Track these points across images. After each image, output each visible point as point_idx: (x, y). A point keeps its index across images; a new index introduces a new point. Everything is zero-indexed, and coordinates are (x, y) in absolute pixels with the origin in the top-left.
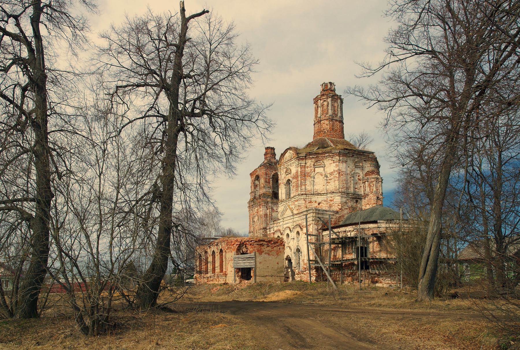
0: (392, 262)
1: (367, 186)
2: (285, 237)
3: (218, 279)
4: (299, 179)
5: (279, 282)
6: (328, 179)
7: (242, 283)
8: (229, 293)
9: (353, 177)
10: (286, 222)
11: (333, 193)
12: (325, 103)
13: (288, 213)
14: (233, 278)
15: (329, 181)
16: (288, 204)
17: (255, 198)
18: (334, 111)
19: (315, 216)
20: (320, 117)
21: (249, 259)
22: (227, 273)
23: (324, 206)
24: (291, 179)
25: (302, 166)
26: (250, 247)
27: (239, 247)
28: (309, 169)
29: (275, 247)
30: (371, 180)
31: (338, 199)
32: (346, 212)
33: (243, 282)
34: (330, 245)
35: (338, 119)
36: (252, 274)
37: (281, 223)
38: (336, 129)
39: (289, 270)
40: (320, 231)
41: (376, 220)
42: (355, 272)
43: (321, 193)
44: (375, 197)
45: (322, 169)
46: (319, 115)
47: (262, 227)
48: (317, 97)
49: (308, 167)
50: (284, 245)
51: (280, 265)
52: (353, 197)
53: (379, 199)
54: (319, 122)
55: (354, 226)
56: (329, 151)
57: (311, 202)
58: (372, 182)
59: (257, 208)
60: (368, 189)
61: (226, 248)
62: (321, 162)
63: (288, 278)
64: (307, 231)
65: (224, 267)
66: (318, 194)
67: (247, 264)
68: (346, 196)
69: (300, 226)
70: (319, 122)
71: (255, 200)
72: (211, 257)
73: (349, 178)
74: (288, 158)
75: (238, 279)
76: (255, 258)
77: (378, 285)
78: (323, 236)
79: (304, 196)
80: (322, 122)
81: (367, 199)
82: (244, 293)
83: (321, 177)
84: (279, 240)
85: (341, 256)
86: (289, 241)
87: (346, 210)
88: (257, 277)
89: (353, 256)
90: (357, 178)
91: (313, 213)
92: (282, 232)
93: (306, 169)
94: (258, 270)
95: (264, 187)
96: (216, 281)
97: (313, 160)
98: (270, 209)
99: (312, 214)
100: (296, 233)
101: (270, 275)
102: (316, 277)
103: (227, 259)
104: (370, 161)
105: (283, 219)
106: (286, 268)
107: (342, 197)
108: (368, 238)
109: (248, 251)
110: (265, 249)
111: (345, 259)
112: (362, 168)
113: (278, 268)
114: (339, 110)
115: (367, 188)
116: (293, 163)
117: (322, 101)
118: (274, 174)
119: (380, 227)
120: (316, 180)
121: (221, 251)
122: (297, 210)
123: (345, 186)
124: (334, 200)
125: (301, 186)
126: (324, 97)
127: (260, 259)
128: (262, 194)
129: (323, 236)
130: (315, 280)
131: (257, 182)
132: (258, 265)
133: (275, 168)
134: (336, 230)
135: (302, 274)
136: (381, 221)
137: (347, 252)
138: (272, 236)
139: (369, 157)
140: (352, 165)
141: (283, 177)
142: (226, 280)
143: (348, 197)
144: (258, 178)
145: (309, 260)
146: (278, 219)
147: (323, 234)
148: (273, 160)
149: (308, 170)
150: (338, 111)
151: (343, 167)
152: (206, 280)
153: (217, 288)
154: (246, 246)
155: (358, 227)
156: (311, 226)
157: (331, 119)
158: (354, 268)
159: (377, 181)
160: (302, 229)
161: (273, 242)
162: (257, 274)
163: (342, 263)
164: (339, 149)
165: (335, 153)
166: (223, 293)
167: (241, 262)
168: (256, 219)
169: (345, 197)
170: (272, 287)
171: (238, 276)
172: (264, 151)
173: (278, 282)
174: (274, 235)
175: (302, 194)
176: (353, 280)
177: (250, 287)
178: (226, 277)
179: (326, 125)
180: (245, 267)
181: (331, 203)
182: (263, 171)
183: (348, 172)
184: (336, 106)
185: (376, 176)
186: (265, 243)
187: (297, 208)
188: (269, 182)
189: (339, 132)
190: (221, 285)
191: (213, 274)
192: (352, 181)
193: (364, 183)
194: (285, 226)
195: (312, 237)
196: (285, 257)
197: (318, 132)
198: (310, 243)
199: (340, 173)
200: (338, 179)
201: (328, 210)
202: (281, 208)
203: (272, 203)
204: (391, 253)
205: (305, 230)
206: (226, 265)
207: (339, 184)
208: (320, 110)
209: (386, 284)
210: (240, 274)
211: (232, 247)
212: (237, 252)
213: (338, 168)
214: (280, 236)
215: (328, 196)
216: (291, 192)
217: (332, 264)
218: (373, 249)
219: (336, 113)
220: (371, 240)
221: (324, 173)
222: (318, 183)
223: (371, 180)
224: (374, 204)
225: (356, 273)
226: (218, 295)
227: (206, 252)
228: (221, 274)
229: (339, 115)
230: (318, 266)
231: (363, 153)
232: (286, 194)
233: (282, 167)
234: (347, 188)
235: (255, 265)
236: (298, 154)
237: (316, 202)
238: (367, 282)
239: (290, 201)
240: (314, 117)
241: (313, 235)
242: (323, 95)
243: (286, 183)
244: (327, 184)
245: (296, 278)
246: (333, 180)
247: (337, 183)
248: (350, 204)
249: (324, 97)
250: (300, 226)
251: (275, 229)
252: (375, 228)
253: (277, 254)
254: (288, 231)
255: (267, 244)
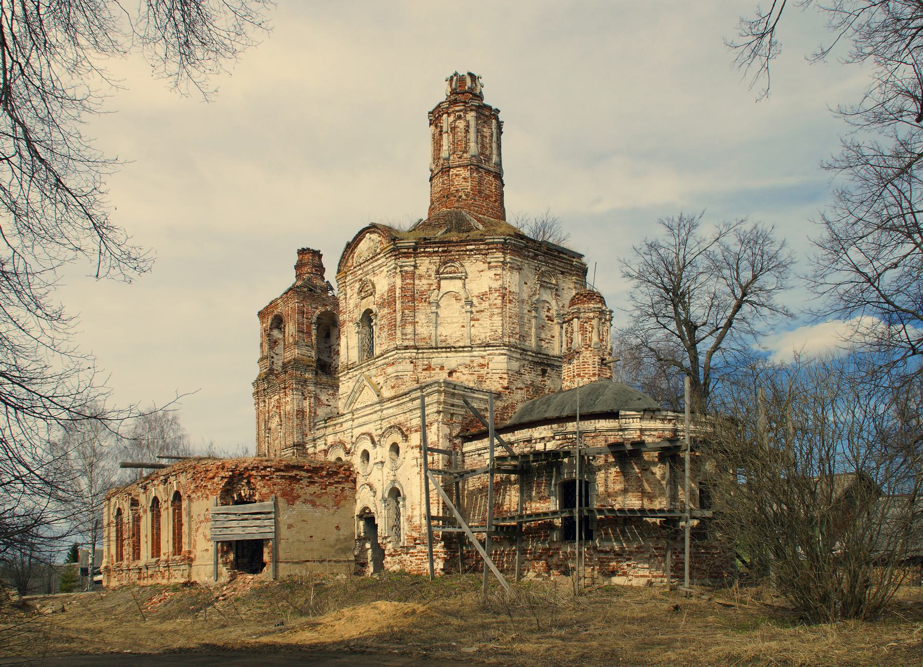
0: (654, 520)
1: (576, 329)
2: (356, 460)
3: (167, 573)
4: (398, 306)
5: (342, 577)
6: (474, 310)
7: (237, 583)
8: (198, 610)
9: (536, 309)
10: (362, 420)
11: (488, 345)
12: (461, 124)
13: (368, 396)
14: (211, 568)
15: (477, 316)
16: (367, 373)
17: (271, 371)
18: (483, 146)
19: (445, 402)
20: (448, 159)
21: (259, 516)
22: (192, 556)
23: (464, 378)
24: (374, 308)
25: (406, 272)
26: (261, 483)
27: (228, 483)
28: (424, 281)
29: (331, 484)
30: (587, 315)
31: (499, 363)
32: (519, 395)
33: (240, 578)
34: (492, 475)
35: (492, 169)
36: (266, 557)
37: (346, 425)
38: (487, 192)
39: (368, 545)
40: (457, 441)
41: (615, 408)
42: (556, 546)
43: (457, 345)
44: (597, 359)
45: (459, 283)
46: (444, 154)
47: (290, 442)
48: (439, 106)
49: (420, 277)
50: (354, 481)
51: (344, 532)
52: (536, 360)
53: (605, 365)
54: (445, 170)
55: (555, 426)
56: (479, 237)
57: (428, 368)
58: (590, 319)
59: (277, 397)
60: (578, 338)
61: (192, 487)
62: (457, 264)
63: (364, 565)
64: (424, 438)
65: (185, 539)
66: (450, 348)
67: (254, 530)
68: (518, 356)
69: (400, 429)
70: (445, 170)
71: (272, 377)
72: (149, 514)
73: (526, 311)
74: (366, 255)
75: (224, 571)
76: (276, 512)
77: (617, 580)
78: (463, 454)
79: (412, 353)
80: (453, 172)
81: (575, 361)
82: (243, 609)
83: (457, 306)
84: (341, 467)
85: (514, 506)
86: (369, 469)
87: (519, 391)
88: (281, 566)
89: (553, 505)
90: (544, 314)
91: (439, 392)
92: (348, 446)
93: (417, 282)
94: (282, 545)
95: (296, 343)
96: (163, 578)
97: (436, 259)
98: (312, 399)
99: (435, 397)
100: (388, 447)
101: (316, 558)
102: (445, 560)
103: (195, 517)
104: (573, 275)
105: (352, 412)
106: (360, 539)
107: (510, 358)
108: (594, 458)
109: (254, 495)
110: (306, 490)
111: (528, 512)
112: (557, 291)
113: (338, 540)
114: (494, 145)
115: (575, 334)
116: (380, 266)
117: (452, 118)
118: (322, 313)
119: (626, 429)
120: (443, 313)
121: (177, 496)
122: (393, 388)
123: (517, 330)
124: (491, 366)
125: (403, 326)
126: (457, 108)
127: (289, 517)
128: (289, 362)
129: (463, 454)
130: (443, 570)
131: (276, 333)
132: (284, 532)
133: (324, 300)
134: (506, 437)
135: (403, 555)
136: (628, 413)
137: (534, 493)
138: (321, 457)
139: (572, 265)
140: (533, 280)
141: (352, 306)
142: (189, 575)
143: (525, 359)
144: (278, 322)
145: (429, 518)
146: (340, 415)
147: (465, 450)
148: (318, 282)
149: (421, 284)
150: (491, 147)
151: (512, 280)
152: (134, 576)
153: (162, 597)
154: (249, 483)
155: (571, 426)
156: (435, 426)
157: (476, 166)
158: (555, 536)
159: (600, 319)
160: (406, 436)
161: (324, 473)
162: (282, 555)
163: (520, 524)
164: (502, 234)
165: (493, 243)
166: (181, 611)
167: (234, 524)
168: (274, 424)
169: (518, 359)
170: (326, 590)
171: (225, 564)
172: (295, 259)
173: (339, 577)
174: (326, 455)
175: (406, 348)
176: (549, 568)
177: (260, 592)
178: (190, 566)
179: (462, 180)
180: (248, 538)
181: (483, 371)
182: (294, 304)
183: (525, 297)
184: (488, 135)
185: (600, 305)
186: (303, 474)
187: (392, 382)
188: (309, 333)
189: (495, 201)
190: (175, 588)
191: (155, 559)
192: (533, 321)
193: (569, 321)
194: (357, 432)
195: (436, 456)
196: (357, 512)
197: (442, 198)
198: (433, 470)
199: (506, 298)
200: (499, 311)
201: (475, 387)
202: (346, 385)
203: (316, 384)
204: (651, 498)
205: (415, 439)
206: (190, 534)
207: (503, 325)
208: (446, 141)
209: (636, 577)
210: (232, 556)
211: (209, 484)
212: (222, 498)
213: (500, 282)
214: (344, 458)
215: (475, 353)
216: (377, 341)
217: (497, 526)
218: (606, 486)
219: (487, 153)
220: (600, 461)
221: (463, 295)
222: (449, 320)
223: (587, 315)
224: (594, 375)
225: (558, 549)
226: (165, 618)
227: (135, 503)
228: (177, 557)
229: (495, 158)
230: (450, 533)
231: (560, 252)
232: (362, 350)
233: (350, 277)
234: (523, 337)
235: (277, 532)
236: (394, 240)
237: (442, 368)
238: (586, 572)
239: (372, 367)
240: (430, 160)
241: (439, 451)
242: (454, 102)
243: (361, 320)
244: (472, 323)
245: (387, 566)
246: (487, 313)
247: (497, 320)
248: (528, 377)
249: (457, 108)
250: (400, 429)
251: (331, 439)
252: (611, 430)
253: (337, 504)
254: (366, 445)
255: (310, 477)
